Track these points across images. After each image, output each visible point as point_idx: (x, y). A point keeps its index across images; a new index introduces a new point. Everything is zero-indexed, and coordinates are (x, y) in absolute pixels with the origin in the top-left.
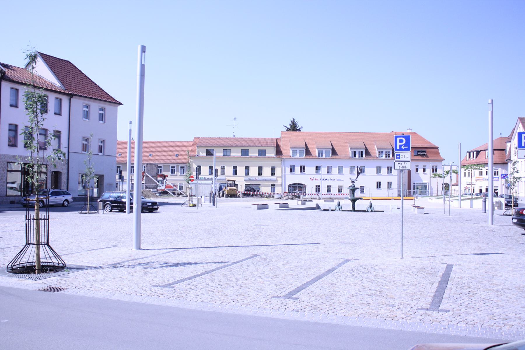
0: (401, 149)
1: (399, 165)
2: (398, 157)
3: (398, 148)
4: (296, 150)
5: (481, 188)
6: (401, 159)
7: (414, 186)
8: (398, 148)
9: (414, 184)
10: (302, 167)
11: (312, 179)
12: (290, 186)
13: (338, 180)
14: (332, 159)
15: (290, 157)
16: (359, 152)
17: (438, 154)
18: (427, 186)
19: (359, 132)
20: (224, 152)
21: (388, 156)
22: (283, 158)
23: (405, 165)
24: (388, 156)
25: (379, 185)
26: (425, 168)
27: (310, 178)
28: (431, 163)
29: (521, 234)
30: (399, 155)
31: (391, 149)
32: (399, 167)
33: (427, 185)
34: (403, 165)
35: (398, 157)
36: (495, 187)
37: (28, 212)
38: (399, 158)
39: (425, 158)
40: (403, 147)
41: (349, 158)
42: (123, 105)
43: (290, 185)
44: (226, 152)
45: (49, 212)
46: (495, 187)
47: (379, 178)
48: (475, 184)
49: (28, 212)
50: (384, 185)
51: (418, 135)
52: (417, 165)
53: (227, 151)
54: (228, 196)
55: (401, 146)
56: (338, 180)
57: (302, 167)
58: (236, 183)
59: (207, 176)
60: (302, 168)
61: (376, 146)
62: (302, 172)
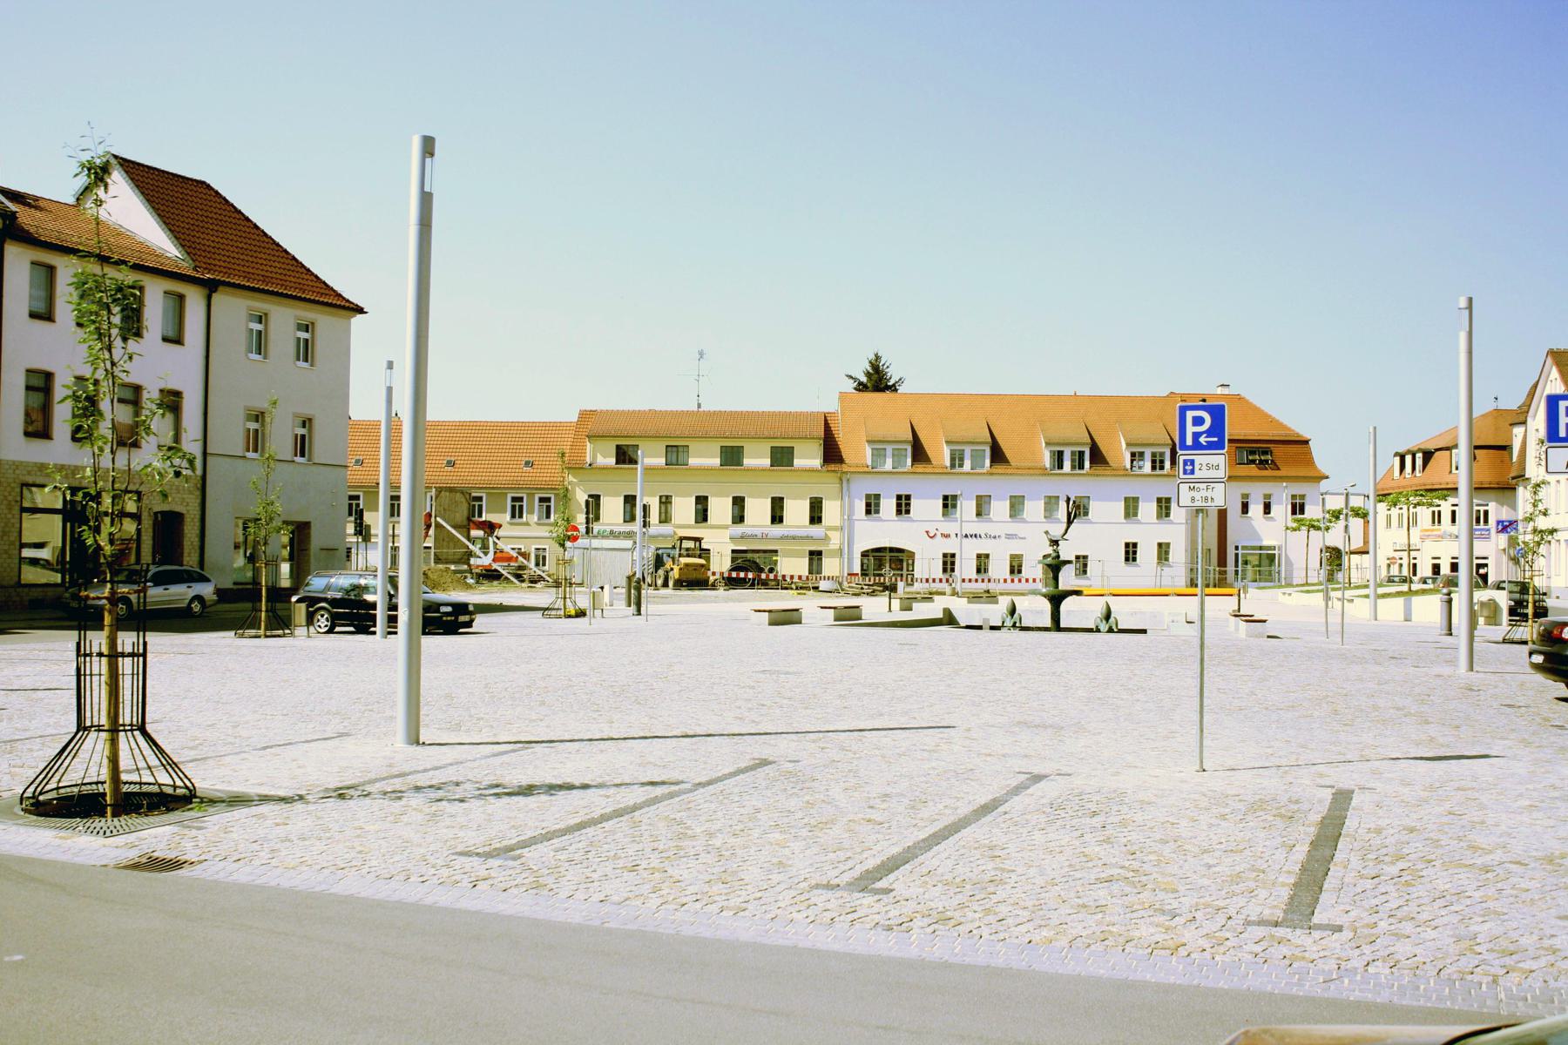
0: (1197, 445)
1: (1193, 493)
2: (1189, 468)
3: (1189, 442)
4: (885, 449)
5: (1436, 561)
6: (1198, 474)
7: (1237, 555)
8: (1189, 442)
9: (1237, 548)
10: (1164, 502)
11: (931, 535)
12: (865, 554)
13: (1009, 536)
15: (866, 469)
16: (1073, 453)
17: (1308, 460)
18: (1275, 554)
20: (669, 454)
23: (1209, 494)
25: (1131, 552)
26: (1270, 503)
27: (927, 532)
30: (1192, 462)
32: (1193, 499)
33: (1276, 552)
34: (1204, 493)
35: (1189, 468)
36: (1477, 558)
37: (82, 632)
38: (1192, 472)
39: (1268, 473)
40: (1203, 440)
41: (1043, 472)
42: (366, 313)
43: (868, 551)
44: (675, 454)
45: (88, 632)
46: (1477, 558)
47: (1131, 533)
48: (1419, 550)
49: (82, 632)
50: (1147, 554)
51: (1247, 402)
52: (1246, 492)
53: (678, 452)
54: (679, 584)
55: (1196, 436)
56: (1009, 536)
57: (1164, 502)
59: (689, 527)
60: (903, 502)
61: (1124, 437)
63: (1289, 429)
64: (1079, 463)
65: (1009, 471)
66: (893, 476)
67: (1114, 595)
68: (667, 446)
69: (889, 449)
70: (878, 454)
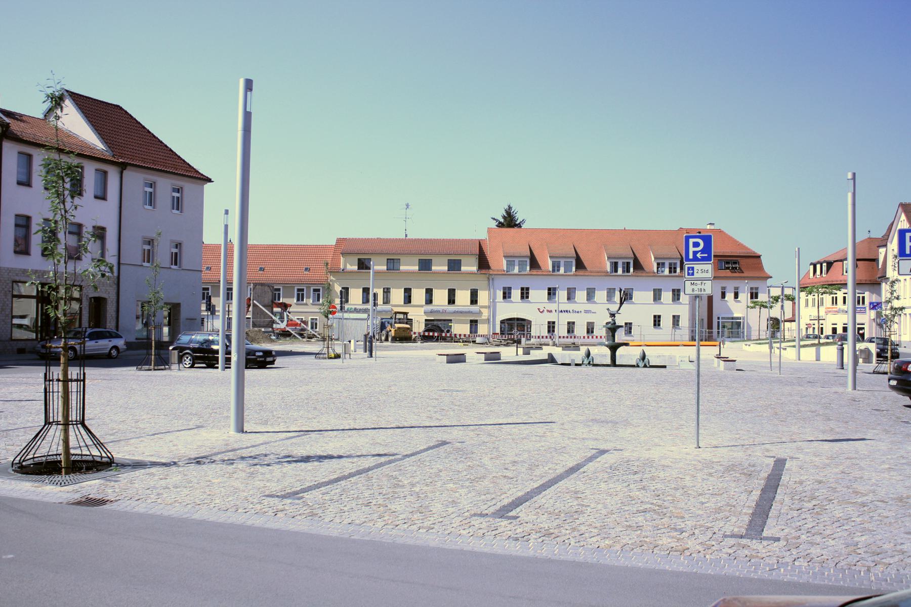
0: (695, 259)
1: (693, 287)
2: (691, 272)
3: (691, 257)
4: (400, 259)
7: (718, 322)
8: (691, 257)
9: (719, 318)
11: (541, 311)
12: (502, 322)
13: (587, 312)
14: (576, 275)
16: (623, 263)
17: (760, 267)
18: (740, 322)
19: (623, 229)
20: (389, 264)
21: (673, 271)
22: (492, 275)
23: (703, 287)
24: (673, 271)
25: (657, 320)
27: (539, 309)
28: (747, 283)
29: (905, 406)
30: (693, 268)
31: (679, 258)
33: (741, 321)
34: (699, 287)
35: (691, 272)
38: (693, 274)
40: (699, 255)
41: (606, 274)
43: (504, 320)
44: (392, 264)
47: (657, 310)
48: (824, 319)
49: (48, 367)
50: (667, 322)
51: (724, 233)
53: (394, 262)
54: (394, 339)
55: (695, 253)
56: (587, 312)
58: (409, 317)
60: (525, 291)
62: (523, 298)
63: (749, 249)
64: (627, 269)
65: (587, 274)
66: (519, 277)
67: (647, 346)
68: (387, 259)
69: (517, 260)
70: (510, 264)
